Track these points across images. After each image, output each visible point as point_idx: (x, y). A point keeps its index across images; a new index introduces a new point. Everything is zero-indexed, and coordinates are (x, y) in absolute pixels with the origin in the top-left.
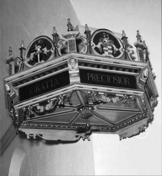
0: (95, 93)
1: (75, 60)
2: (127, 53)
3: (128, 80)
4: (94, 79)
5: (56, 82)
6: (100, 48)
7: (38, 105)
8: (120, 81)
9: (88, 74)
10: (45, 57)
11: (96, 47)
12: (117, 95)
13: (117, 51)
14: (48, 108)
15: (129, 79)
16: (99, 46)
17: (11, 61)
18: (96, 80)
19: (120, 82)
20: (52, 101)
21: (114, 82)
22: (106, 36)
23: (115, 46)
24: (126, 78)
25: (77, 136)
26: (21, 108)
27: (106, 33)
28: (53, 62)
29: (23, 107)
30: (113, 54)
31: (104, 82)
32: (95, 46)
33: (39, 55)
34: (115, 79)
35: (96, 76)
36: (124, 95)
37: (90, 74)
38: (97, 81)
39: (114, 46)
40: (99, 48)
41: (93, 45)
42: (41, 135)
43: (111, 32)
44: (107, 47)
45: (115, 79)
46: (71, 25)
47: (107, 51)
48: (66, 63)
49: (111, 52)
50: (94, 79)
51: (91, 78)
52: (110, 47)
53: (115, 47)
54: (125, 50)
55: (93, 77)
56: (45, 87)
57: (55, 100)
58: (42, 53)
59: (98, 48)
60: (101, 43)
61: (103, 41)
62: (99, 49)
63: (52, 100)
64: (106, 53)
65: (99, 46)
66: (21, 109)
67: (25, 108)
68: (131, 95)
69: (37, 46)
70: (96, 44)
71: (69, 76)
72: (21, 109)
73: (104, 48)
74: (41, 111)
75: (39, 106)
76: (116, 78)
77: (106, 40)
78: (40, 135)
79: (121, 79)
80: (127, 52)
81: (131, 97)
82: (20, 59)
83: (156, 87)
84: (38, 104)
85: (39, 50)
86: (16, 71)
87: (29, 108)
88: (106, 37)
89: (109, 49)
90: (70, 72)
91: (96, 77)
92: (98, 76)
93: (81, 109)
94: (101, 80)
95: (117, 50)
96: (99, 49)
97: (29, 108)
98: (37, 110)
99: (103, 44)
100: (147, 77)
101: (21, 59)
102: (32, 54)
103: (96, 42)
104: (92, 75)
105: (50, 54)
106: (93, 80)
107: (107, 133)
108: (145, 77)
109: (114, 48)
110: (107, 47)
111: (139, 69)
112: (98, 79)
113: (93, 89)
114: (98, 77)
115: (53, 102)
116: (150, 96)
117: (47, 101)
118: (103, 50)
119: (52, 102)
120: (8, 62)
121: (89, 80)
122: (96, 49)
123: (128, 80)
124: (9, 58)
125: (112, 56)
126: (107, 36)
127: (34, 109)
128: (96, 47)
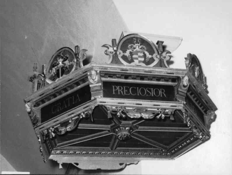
0: (121, 108)
1: (96, 71)
2: (163, 60)
3: (164, 90)
4: (120, 92)
5: (78, 98)
6: (129, 56)
7: (59, 126)
8: (153, 93)
9: (113, 87)
10: (65, 71)
11: (124, 55)
12: (149, 109)
13: (150, 58)
14: (69, 129)
15: (165, 90)
16: (127, 54)
17: (34, 78)
18: (124, 93)
19: (154, 95)
20: (74, 120)
21: (146, 95)
22: (137, 41)
23: (148, 52)
24: (161, 89)
25: (121, 164)
26: (42, 131)
27: (137, 38)
28: (73, 75)
29: (44, 130)
30: (144, 62)
31: (144, 95)
32: (122, 54)
33: (104, 79)
34: (148, 91)
35: (123, 88)
36: (158, 109)
37: (115, 86)
38: (125, 94)
39: (146, 53)
40: (127, 56)
41: (120, 53)
42: (77, 164)
43: (137, 34)
44: (137, 55)
45: (147, 92)
46: (143, 42)
47: (137, 59)
48: (86, 76)
49: (143, 59)
50: (120, 92)
51: (116, 92)
52: (142, 54)
53: (148, 54)
54: (160, 57)
55: (119, 91)
56: (67, 105)
57: (77, 119)
58: (63, 67)
59: (126, 56)
60: (130, 50)
61: (133, 48)
62: (128, 58)
63: (73, 119)
64: (136, 62)
65: (127, 54)
66: (42, 132)
67: (46, 131)
68: (168, 109)
69: (59, 59)
70: (124, 51)
71: (90, 91)
72: (42, 132)
73: (134, 56)
74: (62, 132)
75: (60, 127)
76: (148, 89)
77: (137, 47)
78: (75, 163)
79: (155, 90)
80: (163, 58)
81: (167, 111)
82: (42, 76)
83: (212, 99)
84: (59, 125)
85: (61, 63)
86: (38, 88)
87: (50, 131)
88: (137, 43)
89: (140, 57)
90: (91, 86)
91: (123, 90)
92: (126, 89)
93: (117, 130)
94: (129, 92)
95: (150, 56)
96: (127, 57)
97: (50, 131)
98: (58, 131)
99: (132, 51)
100: (188, 86)
101: (43, 75)
102: (54, 69)
103: (124, 48)
104: (118, 88)
105: (71, 67)
106: (119, 93)
107: (148, 159)
108: (184, 86)
109: (147, 55)
110: (137, 55)
111: (177, 78)
112: (126, 91)
113: (119, 103)
114: (126, 90)
115: (75, 121)
116: (205, 110)
117: (68, 121)
118: (132, 57)
119: (73, 121)
120: (32, 80)
121: (114, 93)
122: (124, 58)
123: (164, 90)
124: (31, 74)
125: (144, 65)
126: (138, 41)
127: (56, 131)
128: (124, 55)
